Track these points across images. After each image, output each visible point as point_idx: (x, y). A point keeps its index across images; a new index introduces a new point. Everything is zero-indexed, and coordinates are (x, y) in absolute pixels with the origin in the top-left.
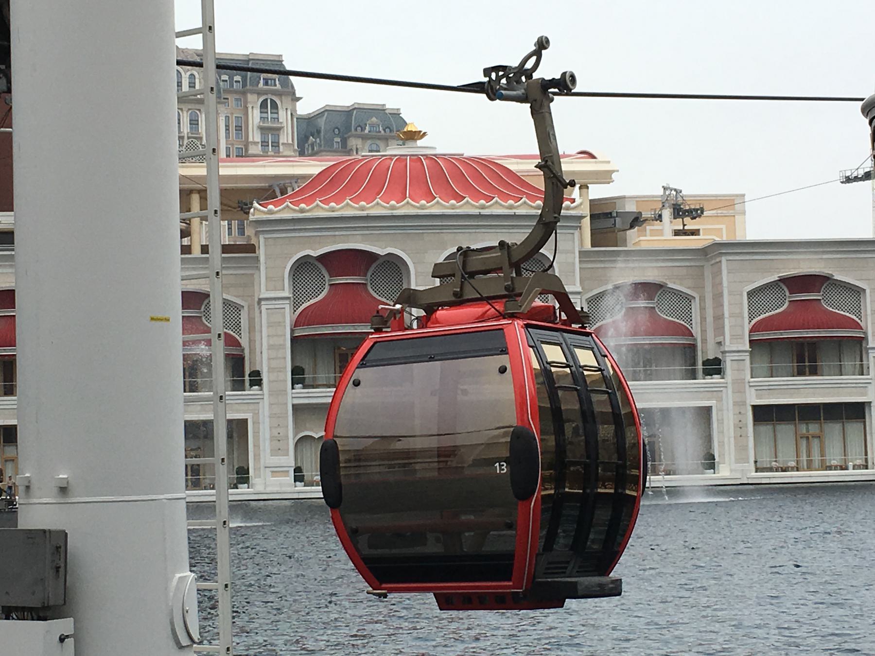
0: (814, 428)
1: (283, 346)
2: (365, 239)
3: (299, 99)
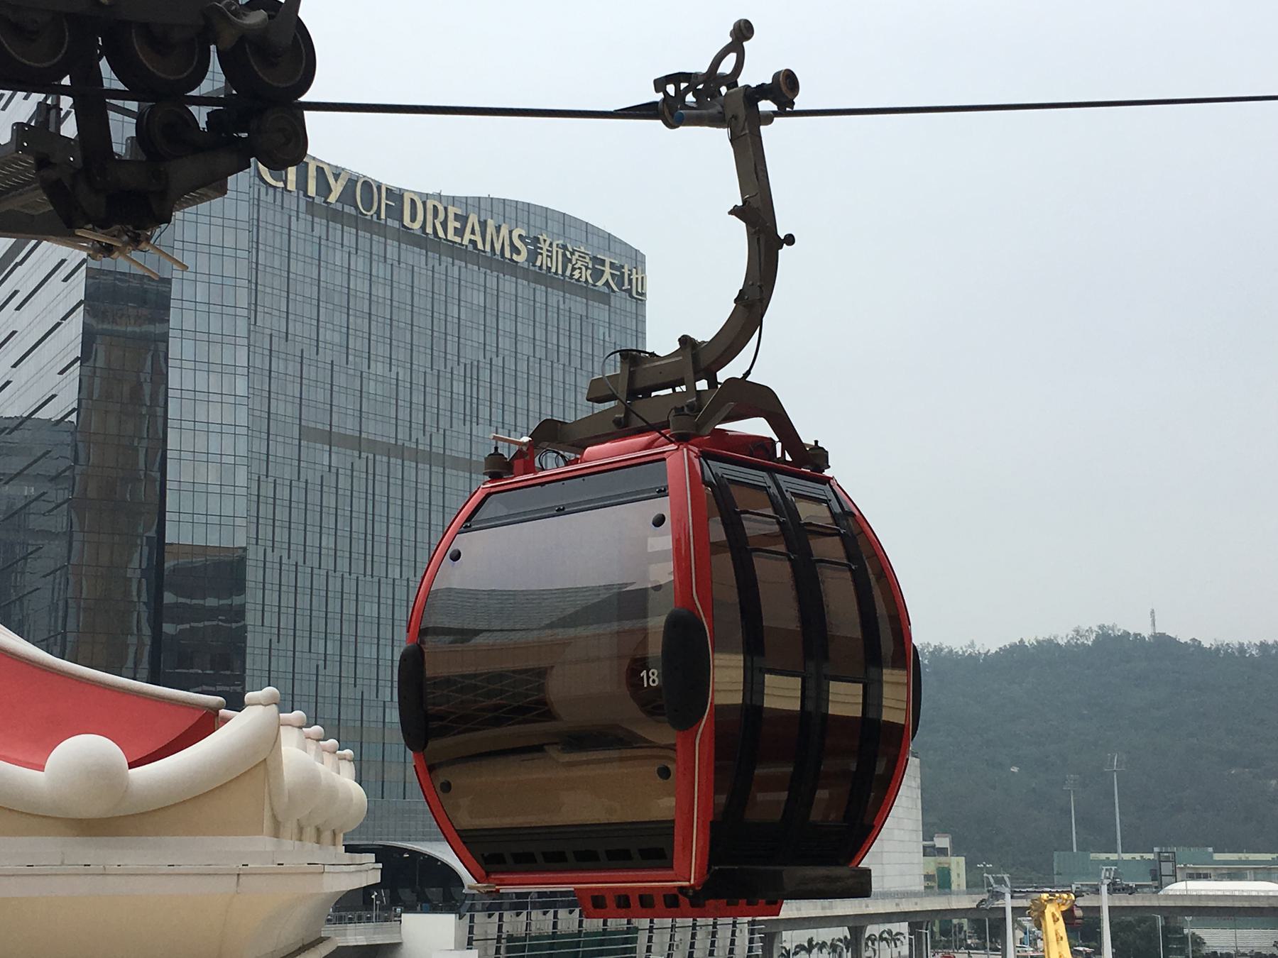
3: (735, 211)
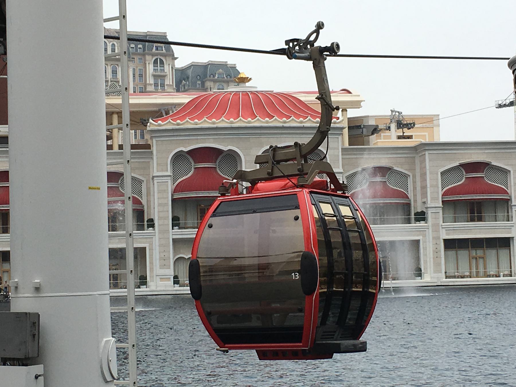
0: (480, 253)
1: (167, 204)
2: (215, 141)
3: (176, 58)
